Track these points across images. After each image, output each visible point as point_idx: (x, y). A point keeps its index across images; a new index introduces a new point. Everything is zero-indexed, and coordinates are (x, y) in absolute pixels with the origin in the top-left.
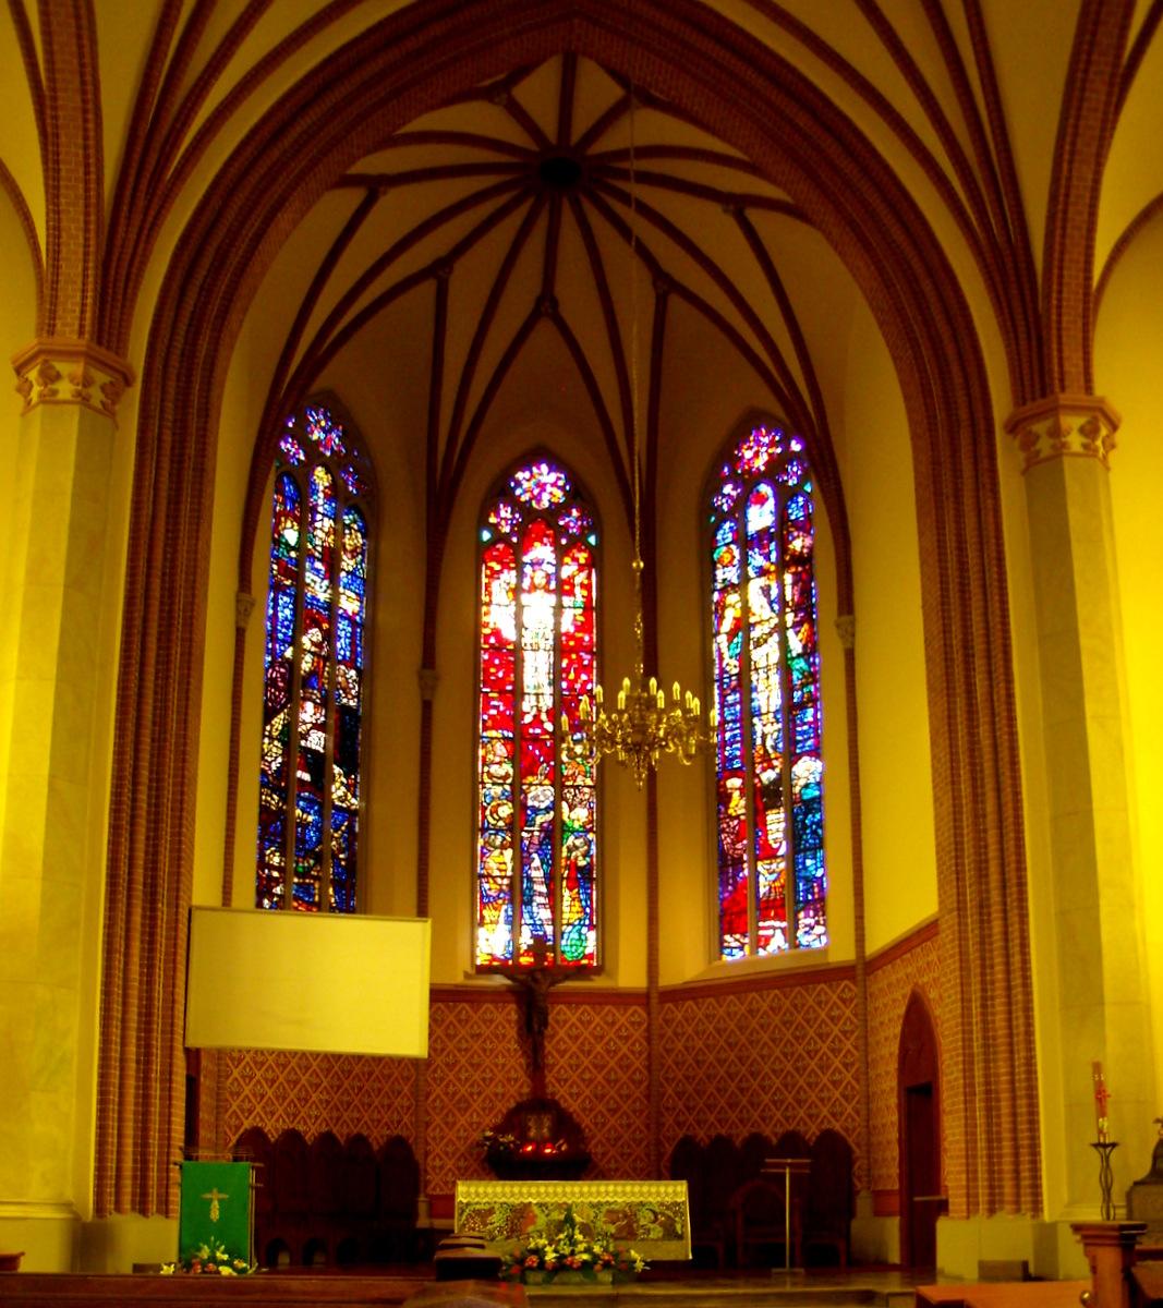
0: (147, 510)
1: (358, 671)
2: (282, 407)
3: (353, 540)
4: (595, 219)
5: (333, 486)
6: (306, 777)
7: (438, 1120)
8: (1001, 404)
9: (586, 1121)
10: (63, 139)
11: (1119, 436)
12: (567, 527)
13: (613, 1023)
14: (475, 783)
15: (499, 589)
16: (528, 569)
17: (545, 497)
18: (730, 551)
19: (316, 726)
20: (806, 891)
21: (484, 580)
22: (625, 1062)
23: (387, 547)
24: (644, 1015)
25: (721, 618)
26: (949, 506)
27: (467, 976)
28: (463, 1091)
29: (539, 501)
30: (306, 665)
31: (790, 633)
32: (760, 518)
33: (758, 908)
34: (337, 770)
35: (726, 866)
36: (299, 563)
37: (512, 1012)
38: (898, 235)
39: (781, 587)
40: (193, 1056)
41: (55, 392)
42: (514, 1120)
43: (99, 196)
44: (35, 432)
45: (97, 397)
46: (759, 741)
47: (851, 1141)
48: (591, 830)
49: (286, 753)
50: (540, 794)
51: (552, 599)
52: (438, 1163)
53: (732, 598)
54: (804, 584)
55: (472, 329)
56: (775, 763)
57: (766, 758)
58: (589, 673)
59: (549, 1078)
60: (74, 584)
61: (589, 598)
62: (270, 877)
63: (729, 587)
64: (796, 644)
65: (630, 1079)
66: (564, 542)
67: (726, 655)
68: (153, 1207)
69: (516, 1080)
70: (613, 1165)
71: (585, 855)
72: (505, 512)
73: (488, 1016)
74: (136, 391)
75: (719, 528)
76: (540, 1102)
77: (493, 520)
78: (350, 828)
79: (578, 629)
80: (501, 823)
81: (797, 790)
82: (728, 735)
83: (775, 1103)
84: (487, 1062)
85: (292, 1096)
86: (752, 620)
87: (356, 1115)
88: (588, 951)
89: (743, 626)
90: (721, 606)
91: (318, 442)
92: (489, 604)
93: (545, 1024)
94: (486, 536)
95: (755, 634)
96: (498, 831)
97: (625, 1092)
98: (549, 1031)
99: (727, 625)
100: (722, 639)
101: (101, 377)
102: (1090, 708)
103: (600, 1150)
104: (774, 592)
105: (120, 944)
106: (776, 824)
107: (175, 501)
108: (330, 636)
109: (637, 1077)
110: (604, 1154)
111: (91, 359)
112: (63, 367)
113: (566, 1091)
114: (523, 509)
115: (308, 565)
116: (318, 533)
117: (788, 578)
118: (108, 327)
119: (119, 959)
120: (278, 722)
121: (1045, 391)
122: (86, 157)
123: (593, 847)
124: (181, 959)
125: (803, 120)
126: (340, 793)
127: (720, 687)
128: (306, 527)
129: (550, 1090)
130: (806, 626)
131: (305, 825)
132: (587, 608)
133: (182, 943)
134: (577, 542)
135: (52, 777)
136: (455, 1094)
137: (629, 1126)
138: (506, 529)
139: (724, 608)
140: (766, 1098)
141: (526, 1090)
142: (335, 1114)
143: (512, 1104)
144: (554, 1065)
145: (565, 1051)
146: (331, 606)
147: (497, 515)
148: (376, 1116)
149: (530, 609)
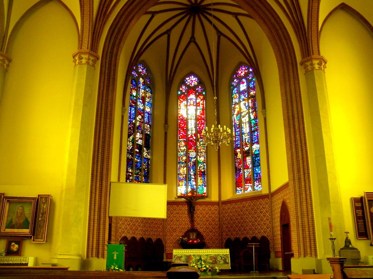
1: (150, 125)
3: (149, 94)
5: (144, 82)
6: (138, 151)
7: (169, 234)
9: (204, 234)
10: (85, 6)
12: (198, 90)
13: (210, 210)
14: (177, 151)
16: (189, 100)
17: (193, 83)
18: (236, 95)
19: (140, 139)
20: (256, 176)
21: (179, 103)
27: (175, 198)
28: (174, 227)
29: (191, 85)
30: (138, 124)
31: (251, 114)
34: (145, 149)
35: (237, 171)
36: (136, 100)
37: (186, 207)
39: (248, 103)
40: (111, 218)
41: (81, 62)
45: (91, 62)
46: (244, 140)
48: (205, 163)
50: (193, 154)
51: (195, 107)
53: (237, 106)
54: (254, 102)
56: (248, 145)
57: (246, 145)
61: (203, 107)
62: (129, 175)
63: (236, 104)
64: (252, 117)
66: (197, 94)
67: (236, 120)
68: (100, 256)
69: (187, 224)
70: (211, 245)
72: (184, 87)
73: (181, 208)
75: (233, 90)
76: (193, 230)
78: (148, 163)
80: (183, 161)
81: (253, 152)
82: (237, 139)
83: (250, 229)
85: (134, 228)
87: (149, 233)
89: (240, 113)
90: (235, 108)
92: (180, 109)
94: (179, 93)
95: (243, 115)
96: (183, 163)
98: (195, 212)
99: (236, 113)
100: (235, 116)
101: (92, 58)
102: (323, 130)
103: (208, 241)
104: (247, 105)
105: (94, 191)
108: (143, 117)
110: (209, 243)
111: (90, 54)
112: (83, 56)
113: (199, 227)
114: (188, 86)
117: (250, 101)
118: (94, 47)
119: (93, 195)
120: (131, 138)
123: (205, 166)
124: (108, 195)
126: (145, 154)
127: (235, 127)
129: (195, 226)
130: (254, 112)
131: (137, 162)
132: (203, 110)
133: (108, 191)
135: (79, 151)
136: (173, 228)
137: (215, 235)
138: (184, 91)
139: (235, 108)
141: (190, 227)
142: (144, 233)
143: (186, 230)
145: (199, 217)
146: (143, 110)
147: (182, 88)
148: (154, 233)
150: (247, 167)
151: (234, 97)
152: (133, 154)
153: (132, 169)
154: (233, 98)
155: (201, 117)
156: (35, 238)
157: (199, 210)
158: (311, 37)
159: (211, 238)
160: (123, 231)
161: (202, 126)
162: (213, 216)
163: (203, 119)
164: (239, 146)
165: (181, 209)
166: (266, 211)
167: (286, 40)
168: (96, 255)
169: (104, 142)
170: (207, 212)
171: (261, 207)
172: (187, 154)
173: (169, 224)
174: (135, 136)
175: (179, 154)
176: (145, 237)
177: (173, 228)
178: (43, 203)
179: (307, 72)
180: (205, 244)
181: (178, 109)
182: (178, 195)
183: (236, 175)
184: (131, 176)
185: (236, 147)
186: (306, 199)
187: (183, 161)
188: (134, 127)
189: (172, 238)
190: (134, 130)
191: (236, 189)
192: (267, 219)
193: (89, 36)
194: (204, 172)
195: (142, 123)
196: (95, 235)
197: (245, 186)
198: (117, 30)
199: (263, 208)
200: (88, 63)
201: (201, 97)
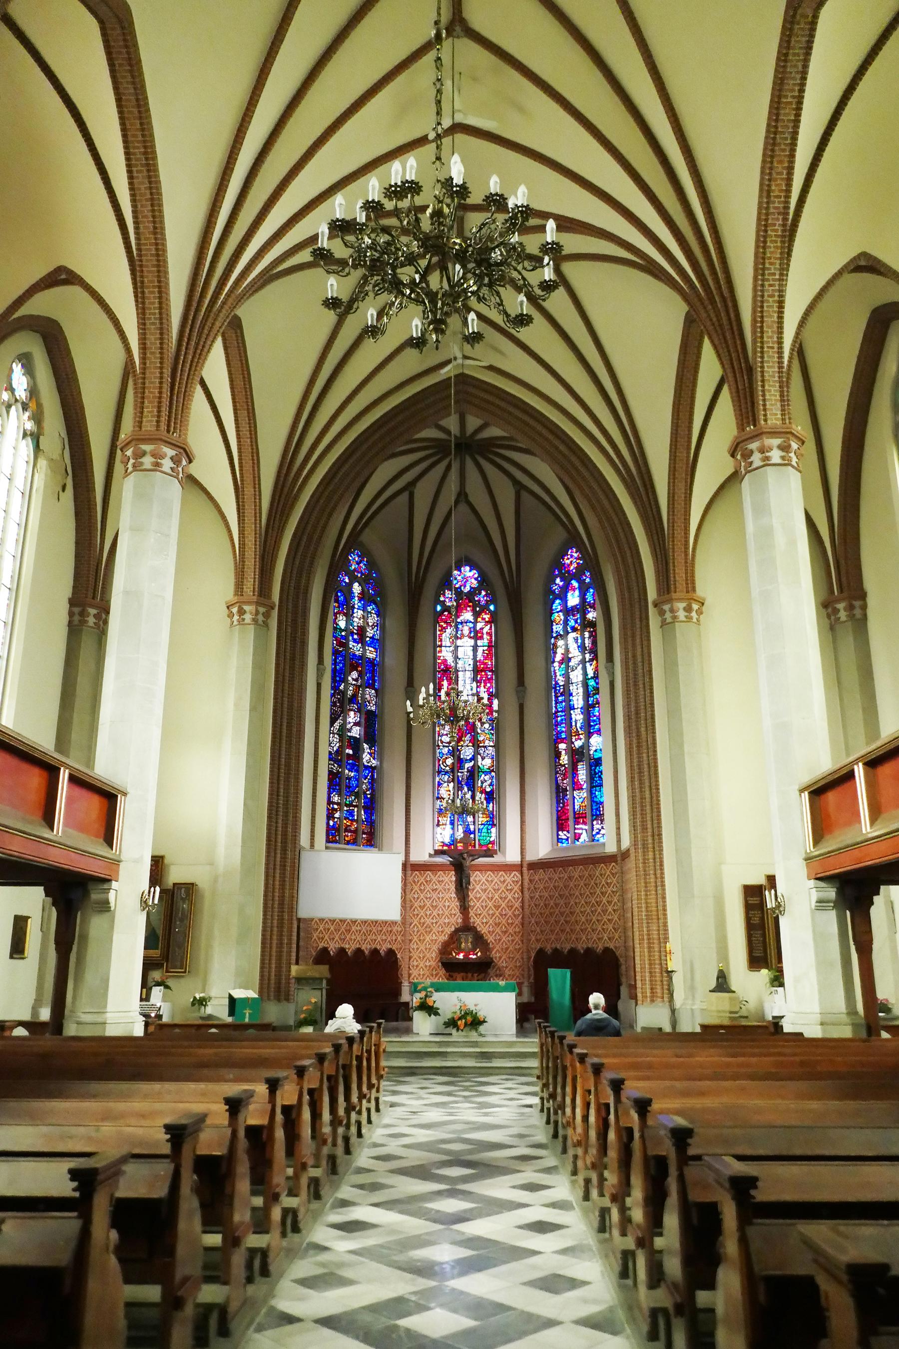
0: (282, 666)
1: (376, 690)
2: (338, 565)
3: (373, 619)
4: (483, 462)
5: (362, 593)
6: (351, 752)
8: (652, 593)
9: (490, 939)
11: (704, 608)
12: (479, 601)
13: (504, 881)
14: (435, 746)
15: (446, 637)
19: (356, 724)
21: (438, 633)
22: (510, 904)
24: (519, 876)
25: (555, 653)
27: (430, 855)
28: (428, 922)
31: (588, 665)
33: (575, 818)
34: (365, 746)
35: (559, 794)
38: (605, 502)
39: (583, 639)
40: (299, 920)
41: (244, 620)
42: (454, 939)
44: (236, 639)
45: (261, 618)
46: (574, 724)
47: (618, 954)
48: (493, 771)
49: (341, 741)
50: (467, 752)
51: (472, 642)
52: (415, 963)
53: (561, 643)
54: (594, 637)
55: (427, 511)
59: (472, 913)
60: (253, 709)
61: (490, 641)
62: (333, 808)
67: (558, 674)
69: (455, 915)
71: (490, 785)
73: (441, 879)
74: (275, 613)
75: (553, 603)
76: (466, 928)
77: (442, 599)
78: (372, 776)
79: (485, 658)
80: (448, 768)
81: (591, 752)
82: (559, 719)
86: (570, 656)
89: (566, 660)
90: (555, 645)
91: (355, 570)
92: (441, 646)
93: (469, 883)
94: (439, 608)
96: (446, 773)
97: (510, 921)
98: (471, 887)
99: (558, 657)
100: (556, 664)
101: (262, 610)
102: (686, 748)
103: (498, 955)
104: (580, 641)
105: (271, 871)
106: (582, 775)
107: (293, 659)
109: (517, 912)
110: (500, 958)
111: (258, 604)
112: (247, 608)
113: (481, 922)
114: (459, 593)
115: (351, 638)
116: (355, 619)
117: (587, 634)
118: (264, 590)
119: (271, 879)
120: (337, 725)
121: (669, 592)
122: (255, 513)
125: (562, 447)
126: (367, 758)
128: (349, 616)
129: (472, 920)
130: (595, 662)
131: (349, 779)
132: (490, 646)
134: (484, 609)
135: (245, 799)
136: (424, 923)
139: (557, 648)
140: (578, 928)
141: (460, 921)
142: (364, 938)
143: (453, 929)
144: (474, 906)
145: (480, 898)
147: (444, 595)
148: (384, 937)
149: (462, 647)
150: (577, 786)
151: (554, 621)
152: (341, 760)
153: (339, 795)
154: (552, 622)
155: (486, 664)
156: (169, 965)
157: (479, 881)
159: (505, 946)
160: (321, 935)
161: (488, 685)
163: (491, 671)
164: (563, 736)
165: (442, 881)
166: (613, 892)
167: (630, 548)
169: (288, 774)
170: (496, 887)
171: (603, 882)
172: (455, 753)
174: (345, 720)
175: (438, 751)
176: (366, 948)
177: (424, 923)
178: (182, 898)
179: (664, 623)
180: (493, 961)
181: (435, 646)
182: (436, 848)
184: (336, 810)
185: (557, 738)
187: (448, 768)
188: (341, 701)
189: (422, 947)
190: (342, 706)
191: (558, 835)
192: (614, 910)
195: (360, 686)
196: (274, 958)
197: (575, 829)
198: (305, 538)
199: (607, 883)
200: (255, 621)
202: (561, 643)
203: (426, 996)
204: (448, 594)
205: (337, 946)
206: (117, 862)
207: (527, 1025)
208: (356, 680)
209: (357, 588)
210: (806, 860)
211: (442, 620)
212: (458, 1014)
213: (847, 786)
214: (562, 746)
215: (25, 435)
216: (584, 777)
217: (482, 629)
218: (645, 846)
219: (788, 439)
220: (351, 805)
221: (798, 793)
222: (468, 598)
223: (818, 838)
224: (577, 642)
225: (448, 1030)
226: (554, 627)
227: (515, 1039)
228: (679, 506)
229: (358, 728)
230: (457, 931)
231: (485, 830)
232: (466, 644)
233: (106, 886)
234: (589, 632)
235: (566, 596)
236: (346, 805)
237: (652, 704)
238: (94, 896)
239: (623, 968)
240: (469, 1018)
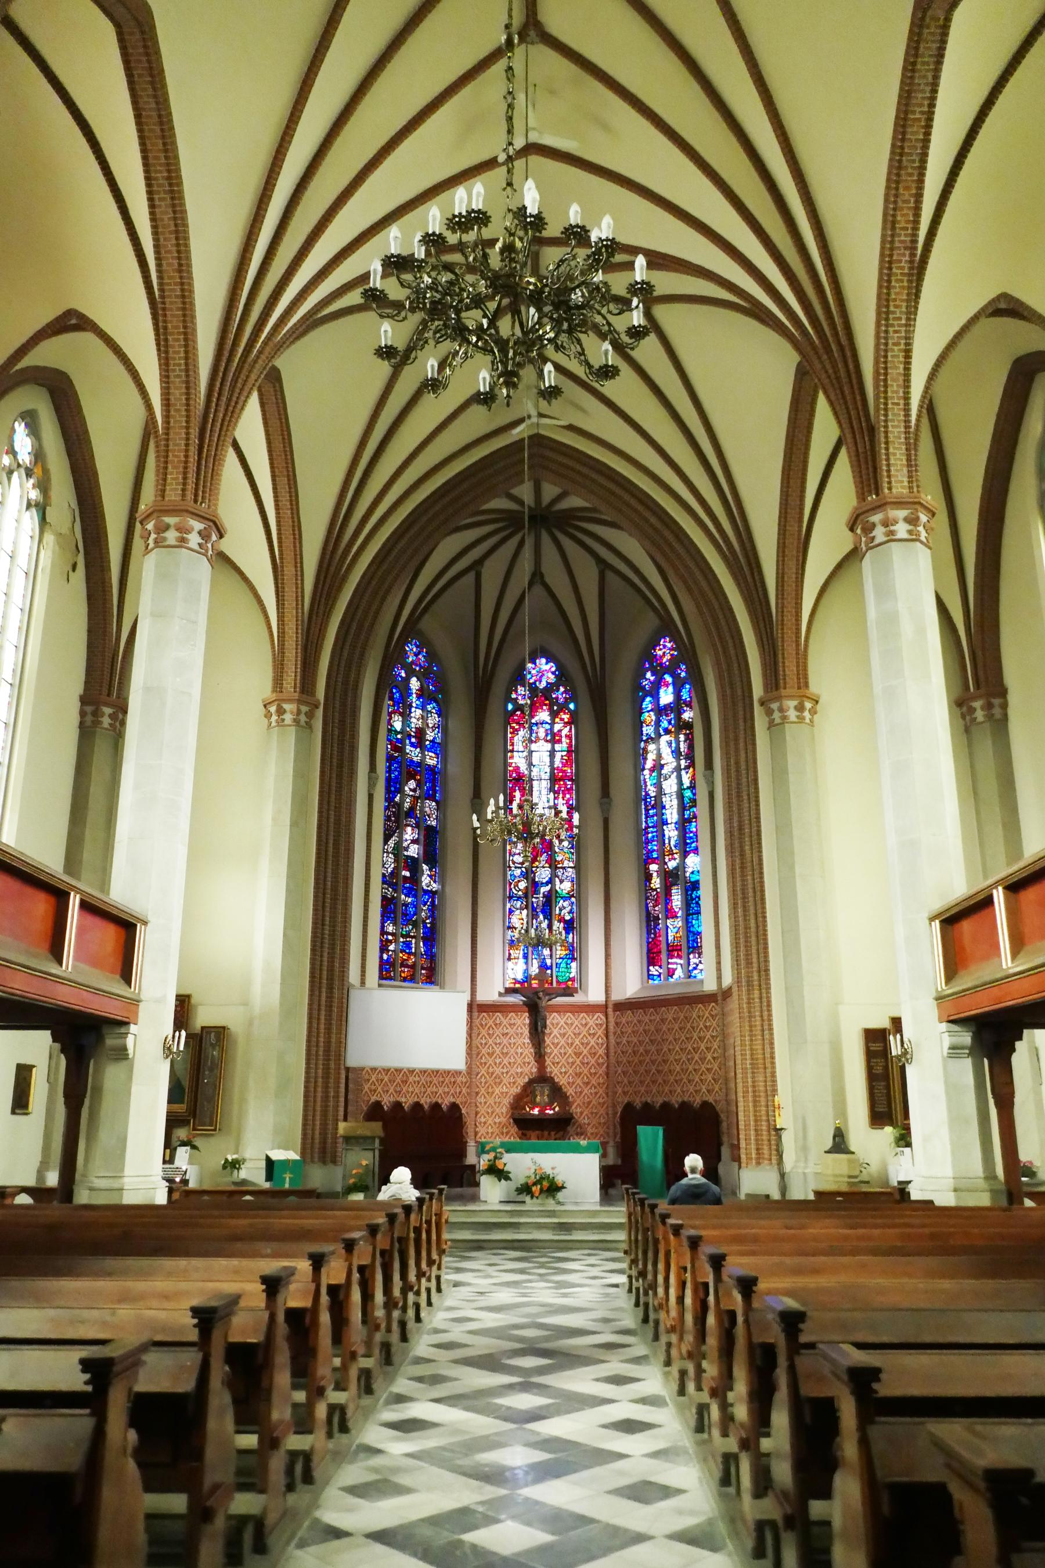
1: (437, 802)
2: (393, 657)
3: (433, 720)
6: (408, 874)
7: (483, 1091)
8: (758, 690)
9: (570, 1091)
10: (286, 589)
12: (557, 698)
13: (586, 1024)
14: (506, 867)
17: (547, 667)
19: (414, 842)
21: (509, 735)
22: (593, 1051)
23: (451, 725)
24: (604, 1018)
25: (645, 759)
26: (732, 744)
27: (500, 994)
31: (683, 772)
32: (666, 696)
33: (668, 950)
34: (425, 867)
35: (650, 923)
37: (525, 1019)
38: (704, 584)
39: (678, 742)
40: (348, 1069)
41: (283, 720)
43: (303, 613)
45: (303, 718)
46: (667, 841)
47: (718, 1108)
48: (573, 896)
49: (396, 861)
50: (543, 874)
51: (549, 746)
52: (483, 1120)
53: (652, 747)
54: (690, 740)
55: (496, 594)
56: (676, 856)
58: (571, 794)
59: (548, 1062)
60: (294, 824)
61: (570, 745)
65: (596, 1062)
68: (328, 1159)
69: (529, 1063)
71: (570, 912)
73: (512, 1021)
75: (643, 700)
76: (542, 1078)
77: (514, 696)
78: (433, 902)
79: (564, 765)
80: (520, 893)
81: (687, 875)
82: (650, 835)
83: (676, 1081)
84: (512, 1051)
86: (662, 762)
88: (572, 976)
89: (658, 767)
91: (413, 662)
92: (512, 751)
93: (545, 1026)
94: (510, 707)
96: (519, 898)
97: (593, 1071)
98: (547, 1031)
99: (649, 764)
100: (646, 772)
101: (304, 709)
102: (798, 870)
103: (579, 1110)
104: (674, 745)
105: (315, 1013)
106: (677, 900)
109: (601, 1061)
110: (581, 1113)
111: (300, 702)
112: (287, 706)
113: (559, 1071)
114: (533, 689)
115: (407, 741)
116: (413, 720)
117: (682, 737)
118: (306, 685)
119: (315, 1022)
120: (391, 843)
121: (777, 688)
125: (653, 520)
127: (645, 804)
128: (406, 716)
129: (549, 1070)
130: (691, 769)
131: (406, 905)
132: (569, 751)
134: (563, 708)
135: (285, 929)
136: (493, 1073)
139: (647, 753)
140: (672, 1079)
141: (535, 1070)
142: (423, 1090)
143: (527, 1080)
144: (551, 1053)
145: (558, 1044)
147: (516, 692)
148: (446, 1090)
151: (645, 722)
152: (396, 883)
153: (395, 924)
154: (642, 723)
155: (565, 772)
156: (197, 1122)
158: (783, 641)
161: (568, 796)
162: (592, 1043)
163: (571, 780)
164: (655, 855)
165: (514, 1024)
166: (713, 1037)
167: (732, 637)
168: (319, 1157)
170: (577, 1031)
171: (701, 1026)
173: (485, 1064)
174: (401, 837)
176: (426, 1101)
177: (493, 1073)
179: (771, 725)
182: (507, 986)
183: (649, 933)
184: (391, 942)
186: (763, 1030)
187: (520, 893)
188: (397, 815)
189: (491, 1101)
191: (648, 970)
192: (714, 1058)
193: (297, 657)
194: (572, 920)
197: (669, 963)
199: (706, 1027)
200: (296, 721)
201: (563, 716)
202: (652, 747)
203: (496, 1158)
204: (521, 690)
205: (392, 1099)
206: (135, 1002)
207: (612, 1191)
208: (414, 790)
209: (415, 684)
210: (937, 999)
211: (514, 721)
212: (533, 1179)
213: (986, 912)
214: (653, 867)
215: (29, 506)
216: (679, 903)
217: (560, 731)
218: (749, 984)
219: (917, 510)
220: (408, 935)
221: (927, 922)
222: (544, 695)
223: (951, 974)
224: (670, 746)
225: (521, 1198)
226: (644, 729)
227: (598, 1208)
228: (790, 587)
229: (416, 846)
230: (531, 1082)
231: (563, 965)
232: (542, 749)
233: (123, 1030)
234: (685, 734)
235: (658, 693)
236: (403, 936)
237: (758, 818)
238: (110, 1042)
239: (724, 1125)
240: (545, 1184)
